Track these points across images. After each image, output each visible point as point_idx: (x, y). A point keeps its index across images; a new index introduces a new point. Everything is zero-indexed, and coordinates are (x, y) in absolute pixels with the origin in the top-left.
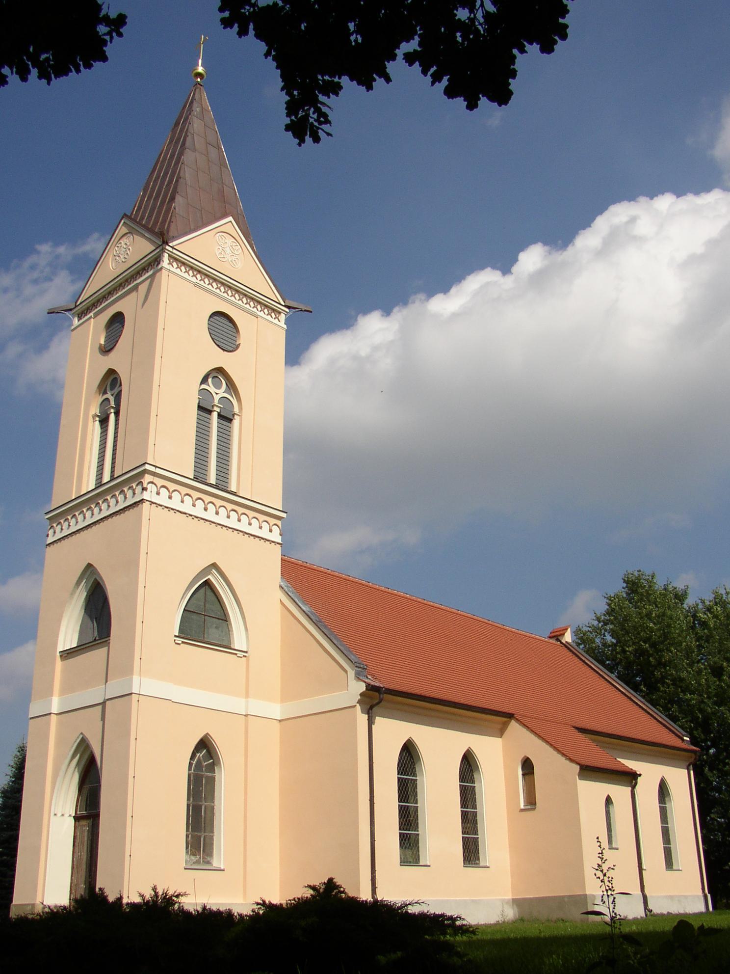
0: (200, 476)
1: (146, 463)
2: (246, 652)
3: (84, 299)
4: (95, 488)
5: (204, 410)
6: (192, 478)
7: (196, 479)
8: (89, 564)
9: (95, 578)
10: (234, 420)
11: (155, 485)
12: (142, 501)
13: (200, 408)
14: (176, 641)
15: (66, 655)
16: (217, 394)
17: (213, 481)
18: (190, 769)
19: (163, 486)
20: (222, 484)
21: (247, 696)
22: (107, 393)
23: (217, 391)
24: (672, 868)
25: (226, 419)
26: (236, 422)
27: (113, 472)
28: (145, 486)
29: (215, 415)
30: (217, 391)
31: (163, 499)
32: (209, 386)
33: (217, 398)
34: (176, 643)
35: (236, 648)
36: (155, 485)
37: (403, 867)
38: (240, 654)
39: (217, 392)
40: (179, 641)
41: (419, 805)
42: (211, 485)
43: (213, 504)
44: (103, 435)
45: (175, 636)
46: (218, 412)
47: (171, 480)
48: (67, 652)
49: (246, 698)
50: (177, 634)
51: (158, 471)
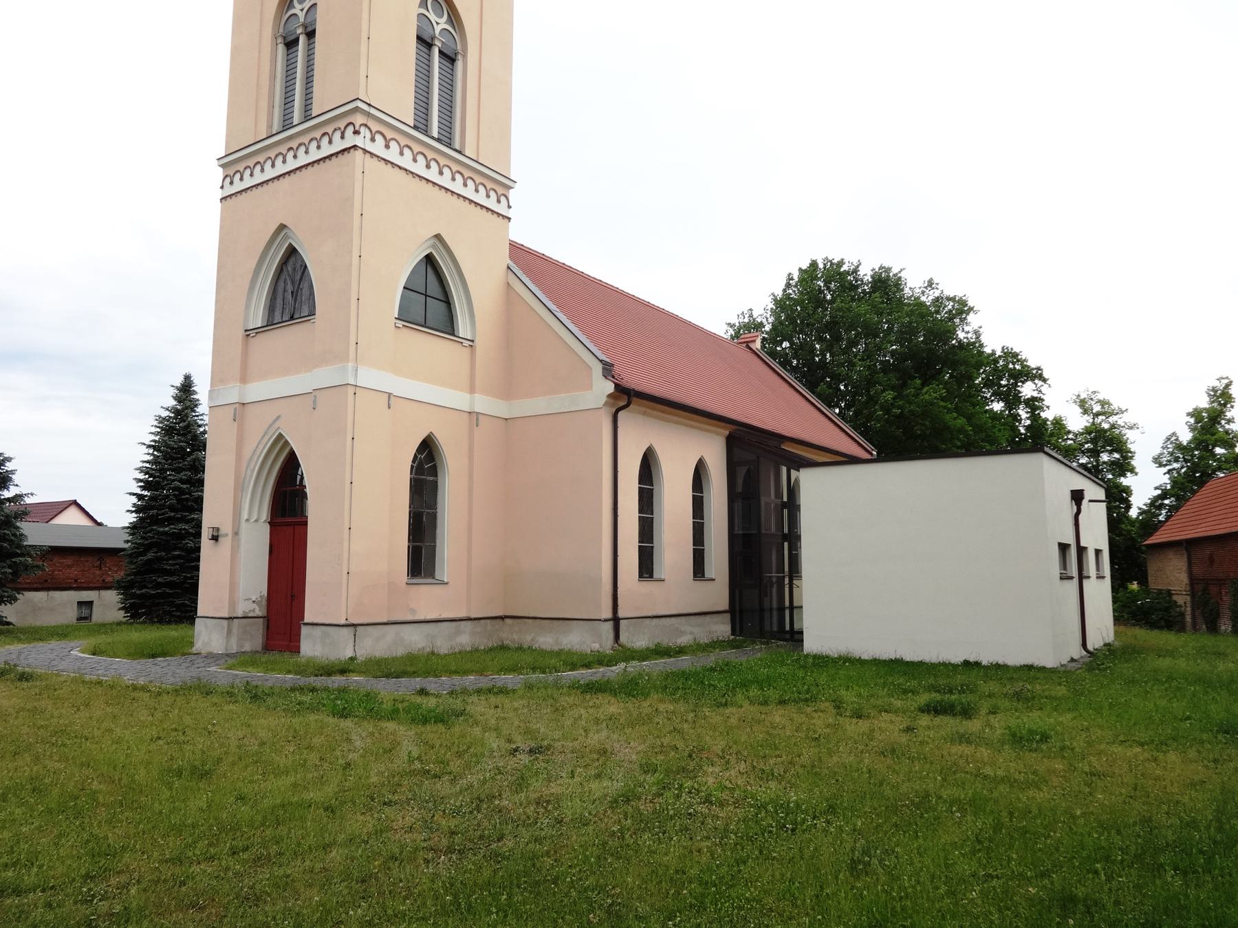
0: (422, 125)
1: (358, 99)
2: (473, 341)
4: (226, 156)
5: (425, 42)
6: (413, 126)
7: (415, 128)
8: (281, 224)
9: (290, 243)
10: (457, 61)
11: (369, 128)
12: (355, 147)
13: (420, 39)
14: (397, 325)
15: (254, 334)
16: (438, 23)
17: (436, 135)
18: (411, 474)
19: (378, 132)
20: (446, 138)
21: (472, 390)
22: (294, 7)
23: (439, 20)
24: (703, 575)
25: (449, 58)
26: (459, 64)
27: (307, 107)
28: (357, 128)
29: (436, 51)
30: (439, 20)
31: (378, 147)
32: (428, 10)
33: (438, 29)
34: (396, 326)
35: (461, 336)
36: (369, 128)
37: (697, 582)
38: (466, 343)
39: (439, 22)
40: (400, 324)
41: (654, 516)
42: (433, 138)
43: (437, 162)
44: (293, 61)
45: (396, 318)
46: (439, 48)
47: (385, 127)
48: (256, 331)
49: (471, 393)
50: (397, 317)
51: (373, 111)
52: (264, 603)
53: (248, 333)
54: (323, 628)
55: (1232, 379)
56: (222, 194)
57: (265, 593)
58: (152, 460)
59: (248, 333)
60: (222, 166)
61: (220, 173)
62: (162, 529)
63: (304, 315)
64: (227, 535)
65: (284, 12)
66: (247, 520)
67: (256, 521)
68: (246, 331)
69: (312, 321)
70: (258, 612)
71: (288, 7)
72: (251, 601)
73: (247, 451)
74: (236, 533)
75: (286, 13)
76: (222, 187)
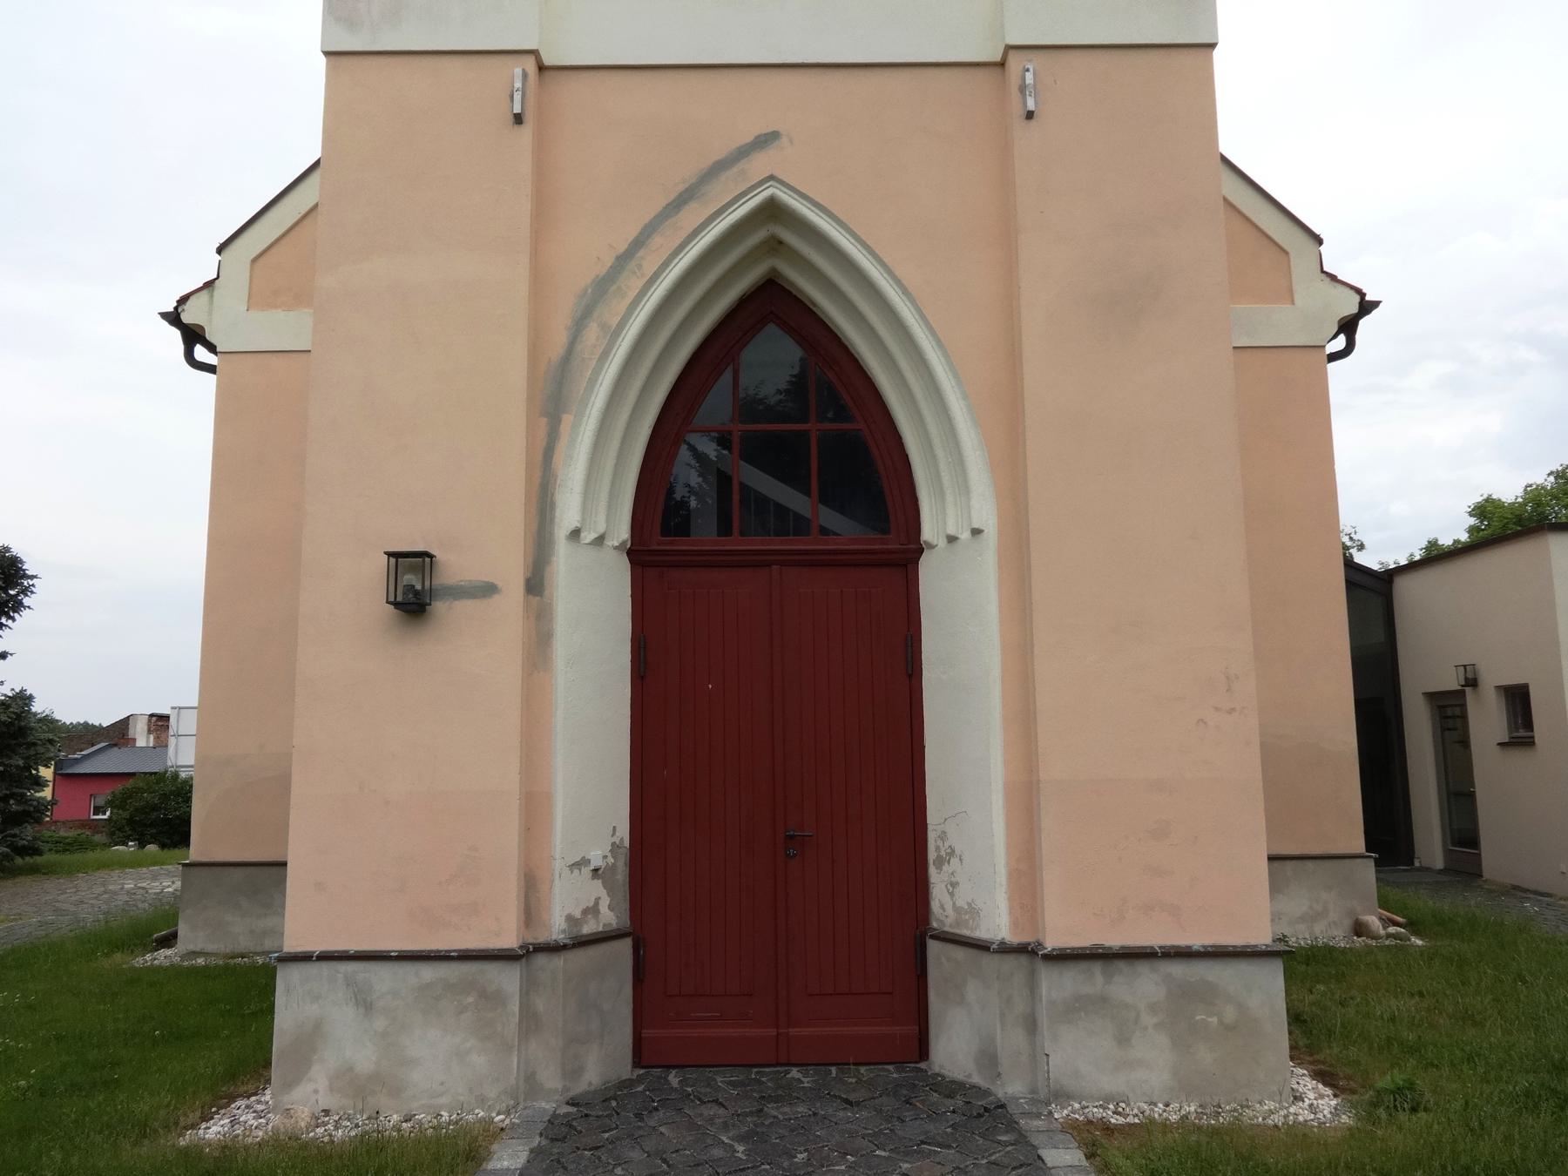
52: (622, 874)
54: (1177, 969)
64: (488, 590)
66: (575, 534)
67: (600, 540)
72: (587, 871)
74: (535, 585)
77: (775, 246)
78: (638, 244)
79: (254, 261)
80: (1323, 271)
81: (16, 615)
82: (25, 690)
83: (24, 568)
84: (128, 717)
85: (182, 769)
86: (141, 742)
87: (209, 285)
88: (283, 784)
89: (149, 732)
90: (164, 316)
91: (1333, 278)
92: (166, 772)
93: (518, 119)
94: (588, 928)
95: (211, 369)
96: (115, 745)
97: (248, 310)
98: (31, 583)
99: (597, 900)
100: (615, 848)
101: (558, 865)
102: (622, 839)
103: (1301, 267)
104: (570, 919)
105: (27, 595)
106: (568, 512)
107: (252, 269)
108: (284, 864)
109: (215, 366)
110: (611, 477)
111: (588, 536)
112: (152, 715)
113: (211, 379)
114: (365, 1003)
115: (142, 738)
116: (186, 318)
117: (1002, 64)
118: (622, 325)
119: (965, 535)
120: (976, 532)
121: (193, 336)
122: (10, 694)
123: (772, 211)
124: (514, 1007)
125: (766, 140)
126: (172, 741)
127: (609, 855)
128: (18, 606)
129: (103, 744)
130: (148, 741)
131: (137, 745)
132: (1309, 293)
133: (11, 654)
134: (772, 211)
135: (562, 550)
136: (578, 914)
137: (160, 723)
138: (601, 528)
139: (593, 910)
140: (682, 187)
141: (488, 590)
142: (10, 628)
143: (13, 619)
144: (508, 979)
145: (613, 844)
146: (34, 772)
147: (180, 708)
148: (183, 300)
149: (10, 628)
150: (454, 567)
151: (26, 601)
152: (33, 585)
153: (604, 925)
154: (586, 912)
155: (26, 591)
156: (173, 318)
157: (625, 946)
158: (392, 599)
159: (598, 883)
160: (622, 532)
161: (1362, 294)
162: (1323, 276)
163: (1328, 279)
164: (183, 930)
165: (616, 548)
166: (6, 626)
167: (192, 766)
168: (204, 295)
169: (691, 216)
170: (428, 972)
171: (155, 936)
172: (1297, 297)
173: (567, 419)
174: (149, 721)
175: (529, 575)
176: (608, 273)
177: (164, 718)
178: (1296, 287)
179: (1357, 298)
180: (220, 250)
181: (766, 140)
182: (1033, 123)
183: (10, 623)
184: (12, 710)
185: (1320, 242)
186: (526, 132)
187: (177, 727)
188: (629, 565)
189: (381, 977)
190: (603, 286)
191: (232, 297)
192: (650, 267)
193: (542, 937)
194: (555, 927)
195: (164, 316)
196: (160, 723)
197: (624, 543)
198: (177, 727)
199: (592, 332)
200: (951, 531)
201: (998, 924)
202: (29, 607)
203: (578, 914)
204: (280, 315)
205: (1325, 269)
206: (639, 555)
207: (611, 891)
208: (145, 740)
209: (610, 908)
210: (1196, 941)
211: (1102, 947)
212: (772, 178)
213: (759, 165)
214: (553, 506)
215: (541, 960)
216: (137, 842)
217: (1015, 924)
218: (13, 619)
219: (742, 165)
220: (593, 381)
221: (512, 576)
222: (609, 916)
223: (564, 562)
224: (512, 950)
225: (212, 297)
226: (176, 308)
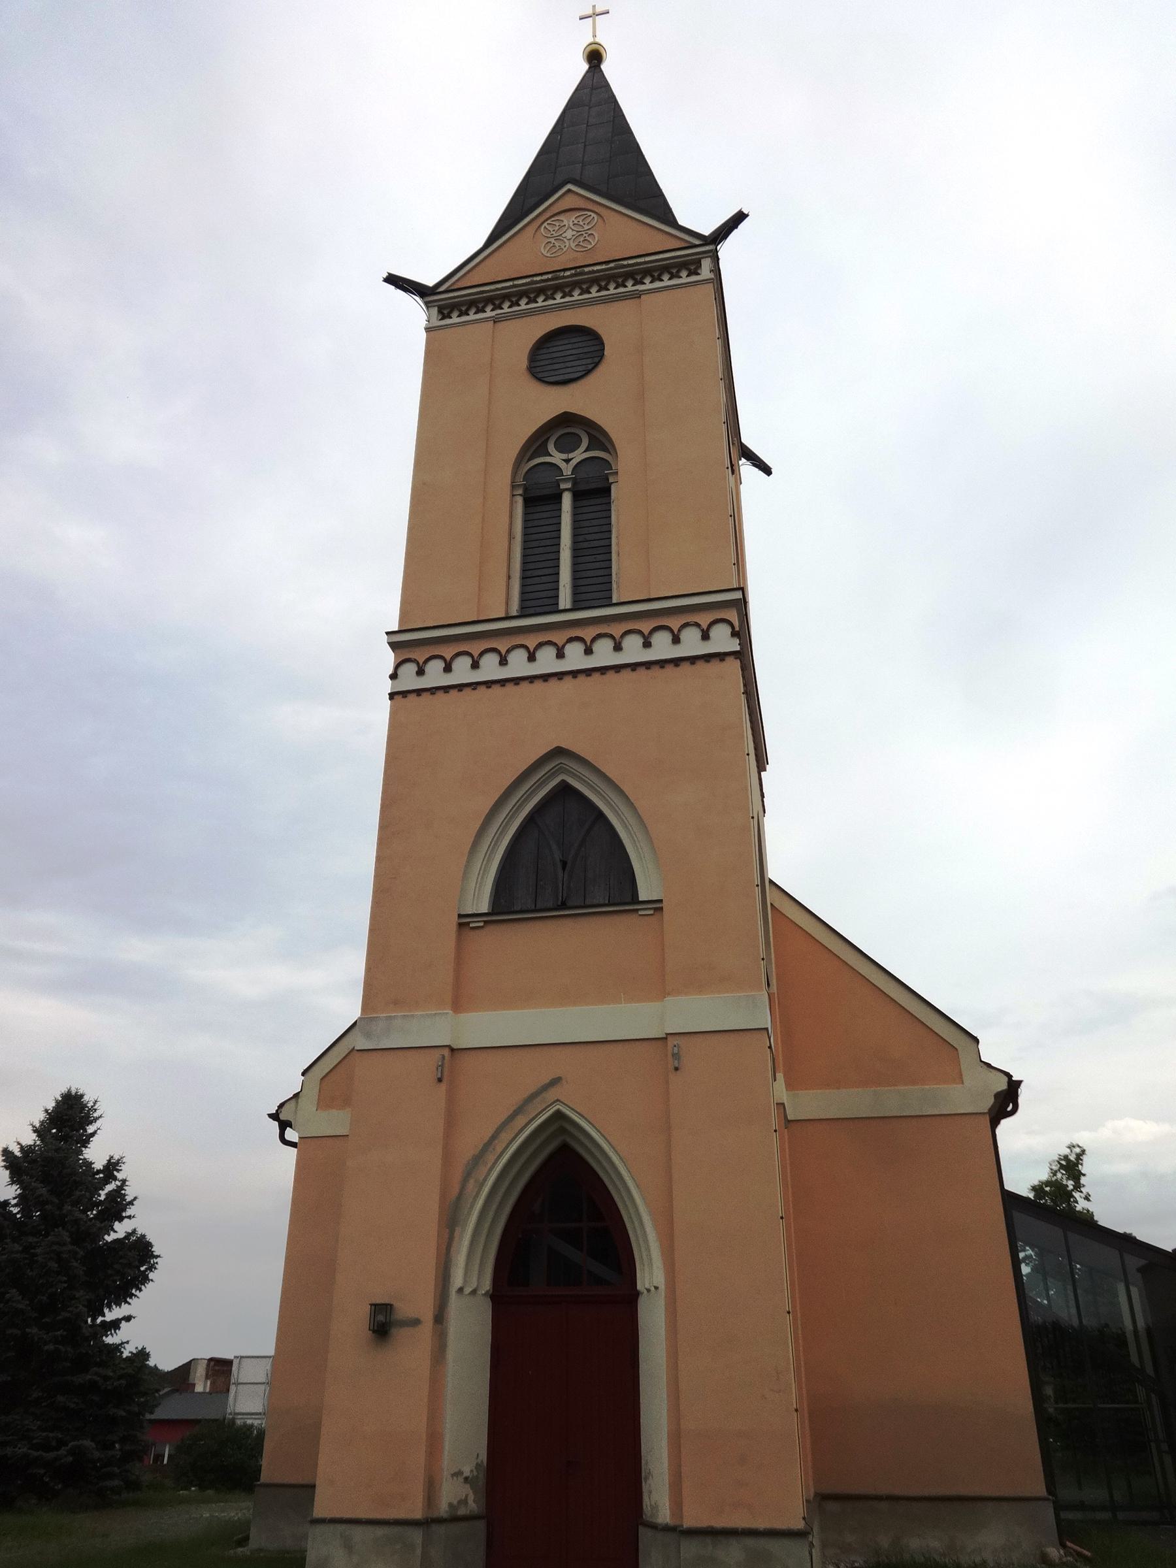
3: (455, 287)
52: (482, 1482)
53: (465, 922)
54: (750, 1542)
55: (1085, 1148)
56: (391, 688)
57: (484, 1457)
58: (18, 1157)
59: (465, 922)
60: (394, 646)
61: (389, 659)
62: (800, 1335)
63: (595, 902)
64: (416, 1322)
65: (527, 458)
66: (461, 1290)
67: (474, 1292)
68: (460, 916)
69: (640, 913)
70: (473, 1506)
71: (534, 452)
72: (461, 1479)
73: (469, 1141)
74: (440, 1318)
75: (529, 460)
76: (393, 677)
77: (563, 1130)
78: (494, 1137)
79: (322, 1079)
80: (981, 1061)
81: (143, 1287)
82: (145, 1348)
83: (153, 1250)
84: (191, 1361)
85: (240, 1417)
86: (199, 1388)
87: (296, 1096)
88: (318, 1425)
89: (207, 1377)
90: (270, 1116)
91: (989, 1065)
92: (224, 1419)
93: (440, 1080)
94: (462, 1512)
95: (293, 1145)
96: (177, 1390)
97: (317, 1110)
98: (155, 1261)
99: (467, 1496)
100: (478, 1466)
101: (446, 1474)
102: (482, 1461)
103: (965, 1060)
104: (451, 1505)
105: (152, 1271)
106: (457, 1279)
107: (320, 1083)
108: (313, 1486)
109: (296, 1143)
110: (463, 1271)
111: (468, 1290)
112: (211, 1360)
113: (293, 1152)
114: (349, 1547)
115: (201, 1385)
116: (282, 1117)
117: (666, 1038)
118: (485, 1180)
119: (653, 1289)
120: (656, 1288)
121: (284, 1125)
122: (135, 1352)
123: (559, 1115)
124: (419, 1552)
125: (555, 1082)
126: (233, 1388)
127: (475, 1471)
128: (145, 1279)
129: (166, 1390)
130: (205, 1387)
131: (196, 1391)
132: (973, 1078)
133: (134, 1318)
134: (559, 1115)
135: (454, 1301)
136: (455, 1502)
137: (220, 1368)
138: (474, 1285)
139: (464, 1502)
140: (515, 1108)
141: (416, 1322)
142: (138, 1297)
143: (141, 1290)
144: (416, 1536)
145: (477, 1464)
146: (141, 1417)
147: (242, 1357)
148: (281, 1106)
149: (138, 1297)
150: (404, 1310)
151: (151, 1276)
152: (157, 1263)
153: (470, 1511)
154: (460, 1502)
155: (152, 1268)
156: (274, 1117)
157: (481, 1525)
158: (371, 1328)
159: (468, 1486)
160: (487, 1285)
161: (1009, 1076)
162: (982, 1064)
163: (985, 1067)
164: (253, 1533)
165: (483, 1295)
166: (136, 1296)
167: (260, 1414)
168: (293, 1102)
169: (520, 1121)
170: (380, 1531)
171: (235, 1539)
172: (965, 1078)
173: (458, 1230)
174: (208, 1365)
175: (436, 1313)
176: (480, 1153)
177: (227, 1363)
178: (964, 1073)
179: (1006, 1079)
180: (303, 1074)
181: (555, 1082)
182: (678, 1072)
183: (137, 1293)
184: (135, 1364)
185: (976, 1040)
186: (443, 1087)
187: (238, 1376)
188: (491, 1304)
189: (358, 1532)
190: (477, 1159)
191: (308, 1105)
192: (499, 1149)
193: (435, 1515)
194: (443, 1509)
195: (270, 1116)
196: (217, 1368)
197: (487, 1292)
198: (238, 1376)
199: (471, 1184)
200: (647, 1286)
201: (664, 1516)
202: (152, 1280)
203: (455, 1502)
204: (334, 1112)
205: (983, 1060)
206: (497, 1298)
207: (475, 1493)
208: (202, 1386)
209: (474, 1501)
210: (761, 1524)
211: (712, 1527)
212: (558, 1100)
213: (551, 1095)
214: (449, 1276)
215: (435, 1528)
216: (197, 1488)
217: (673, 1515)
218: (141, 1290)
219: (544, 1095)
220: (472, 1207)
221: (428, 1316)
222: (473, 1506)
223: (455, 1303)
224: (420, 1520)
225: (297, 1102)
226: (277, 1111)
